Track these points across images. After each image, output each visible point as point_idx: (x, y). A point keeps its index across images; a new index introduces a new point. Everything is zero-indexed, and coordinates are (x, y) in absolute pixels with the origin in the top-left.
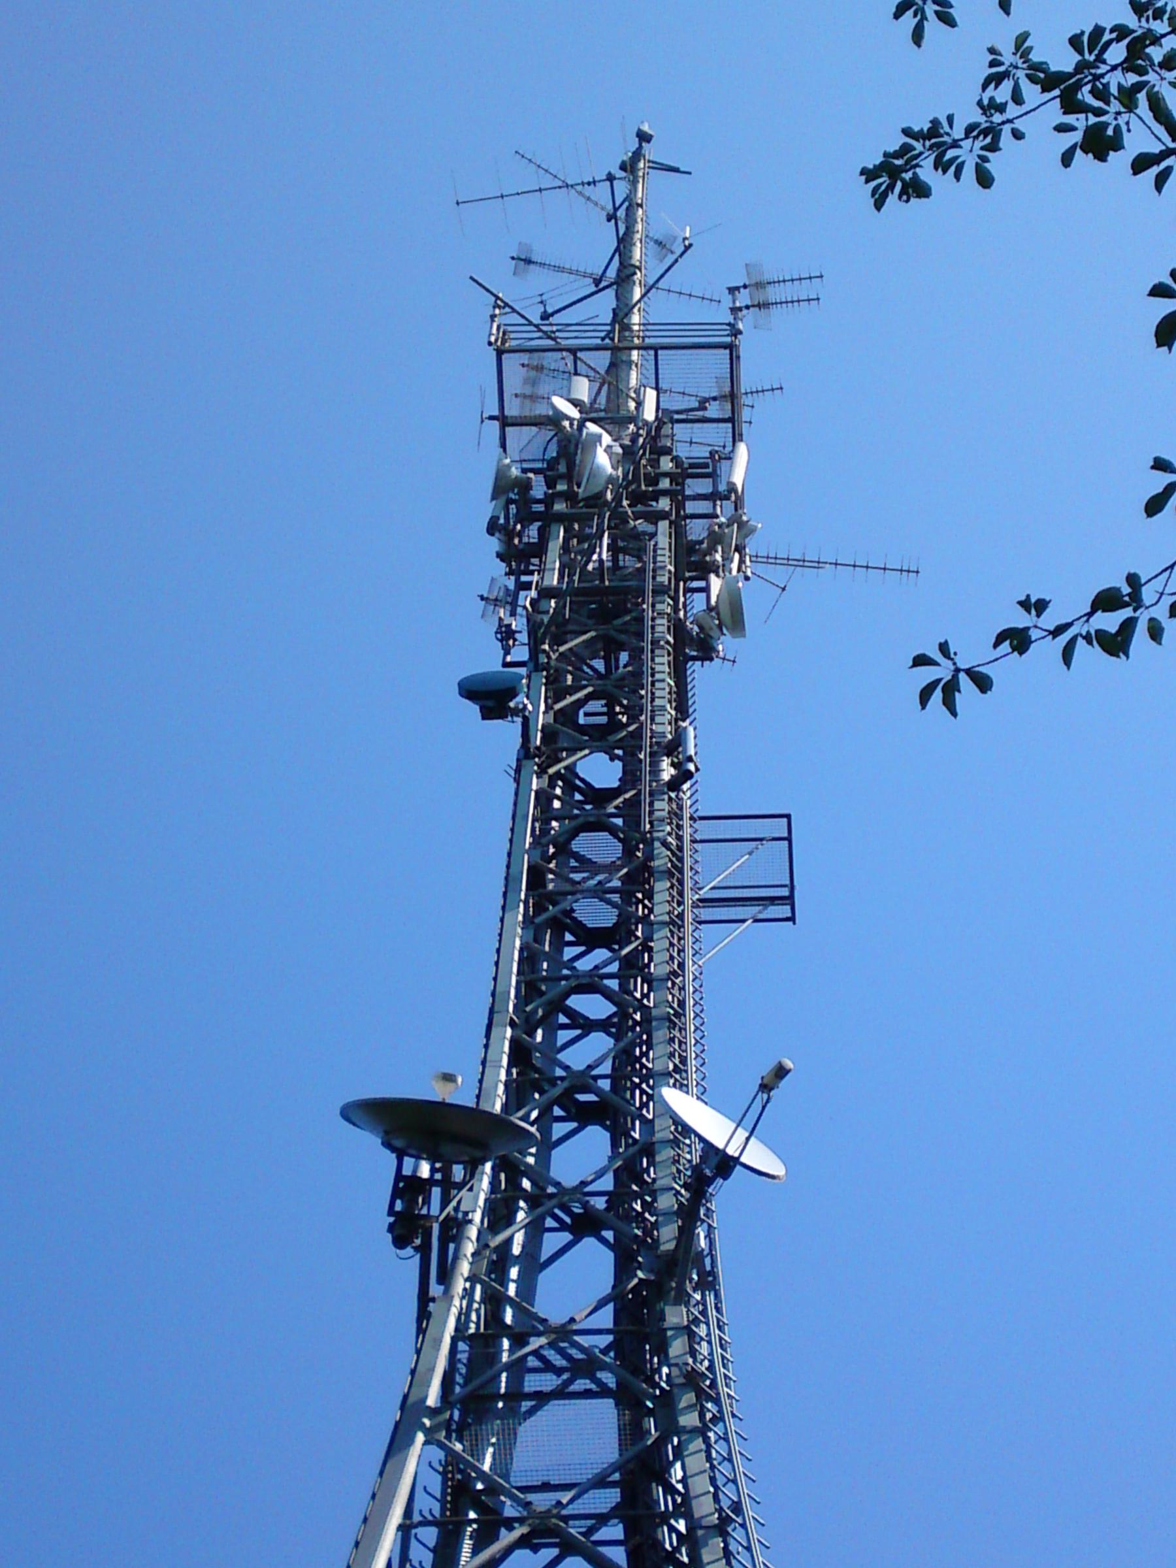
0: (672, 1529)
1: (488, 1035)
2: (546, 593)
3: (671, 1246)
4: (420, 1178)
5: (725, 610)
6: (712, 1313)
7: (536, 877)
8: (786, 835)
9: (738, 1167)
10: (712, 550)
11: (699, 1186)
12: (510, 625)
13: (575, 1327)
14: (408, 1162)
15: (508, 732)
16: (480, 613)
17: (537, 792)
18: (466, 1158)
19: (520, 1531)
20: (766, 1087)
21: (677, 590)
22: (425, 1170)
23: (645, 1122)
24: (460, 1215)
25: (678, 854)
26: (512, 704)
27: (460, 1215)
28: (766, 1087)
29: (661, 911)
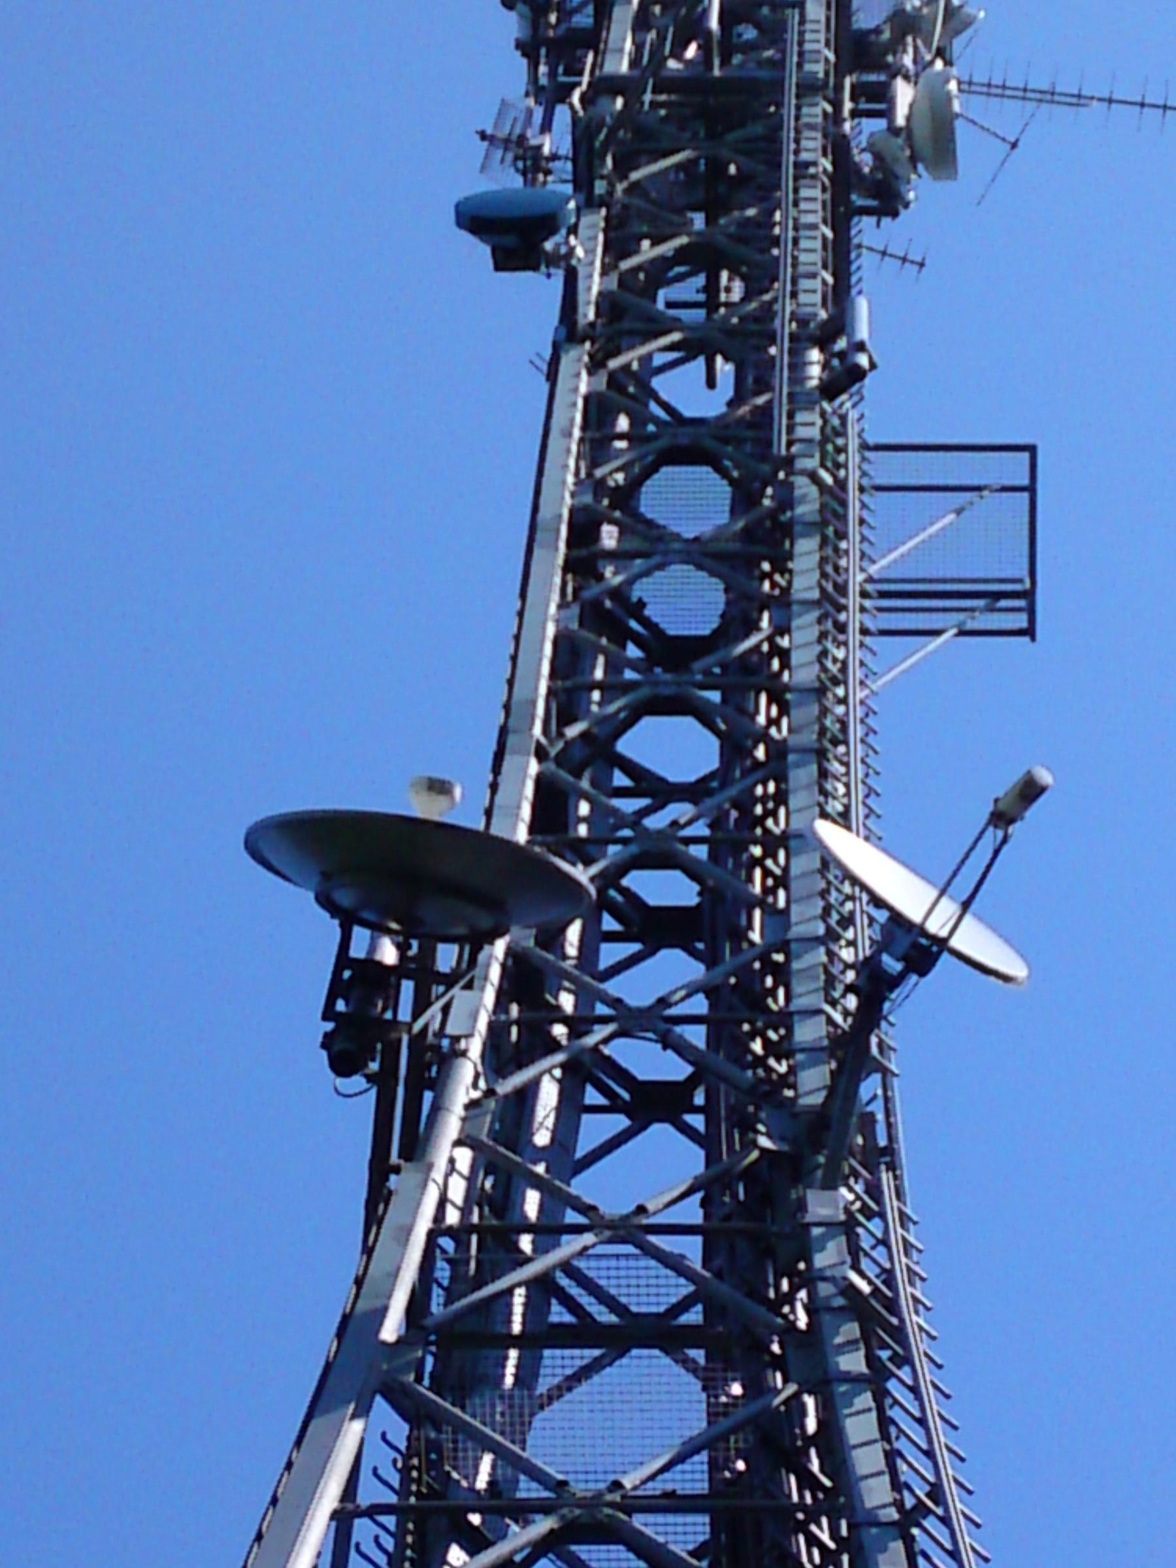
0: (813, 1540)
1: (497, 768)
2: (605, 86)
3: (818, 1099)
4: (380, 964)
5: (922, 133)
6: (891, 1203)
7: (583, 529)
8: (1026, 482)
9: (945, 956)
10: (897, 44)
11: (875, 988)
12: (539, 148)
13: (645, 1221)
14: (360, 936)
15: (540, 291)
16: (479, 165)
17: (587, 399)
18: (461, 930)
19: (543, 1525)
20: (1002, 818)
21: (839, 88)
22: (388, 954)
23: (771, 912)
24: (445, 1043)
25: (836, 495)
26: (548, 246)
27: (445, 1043)
28: (1002, 818)
29: (805, 579)
